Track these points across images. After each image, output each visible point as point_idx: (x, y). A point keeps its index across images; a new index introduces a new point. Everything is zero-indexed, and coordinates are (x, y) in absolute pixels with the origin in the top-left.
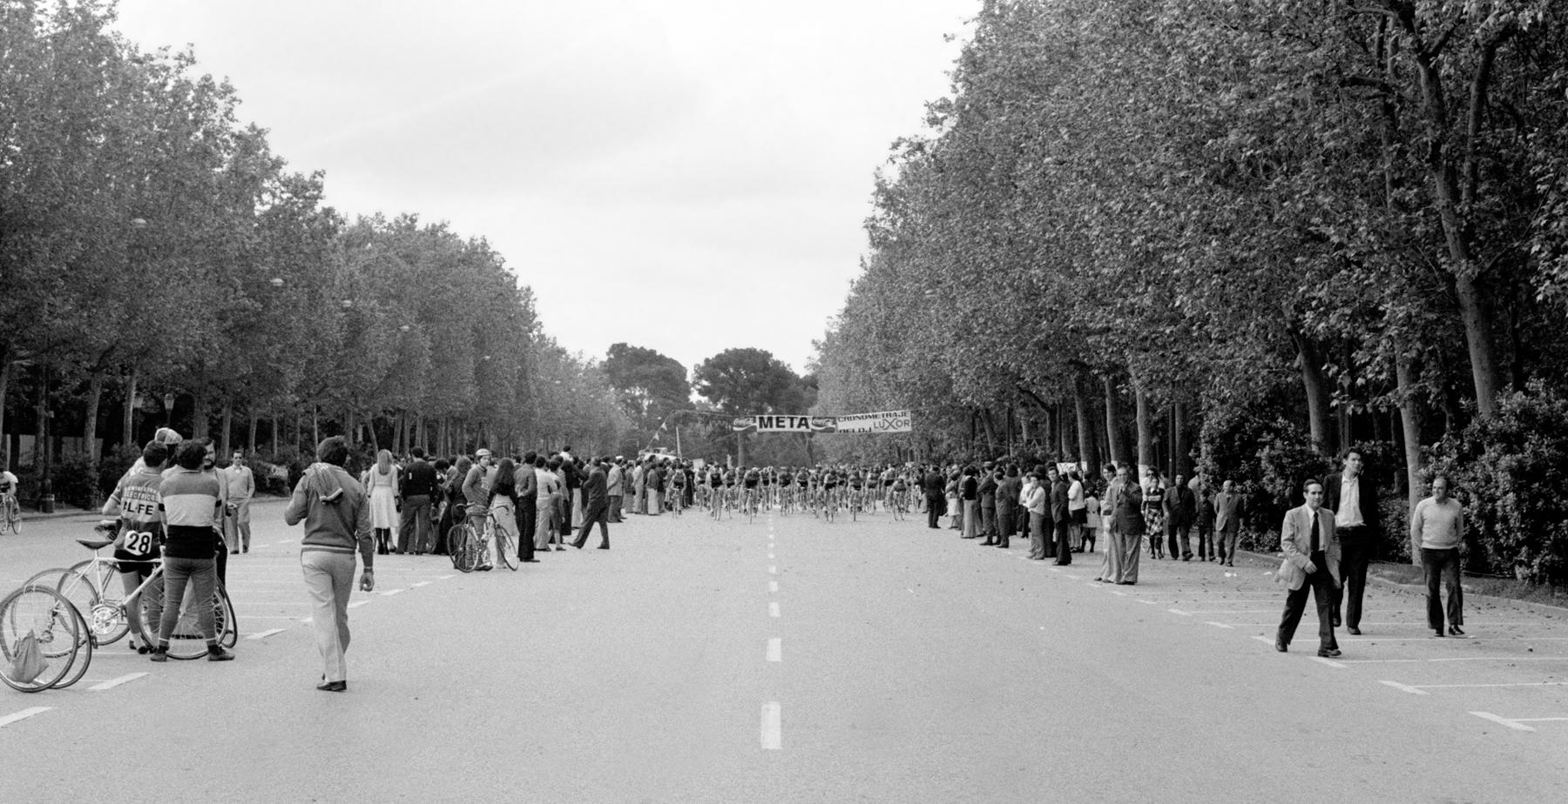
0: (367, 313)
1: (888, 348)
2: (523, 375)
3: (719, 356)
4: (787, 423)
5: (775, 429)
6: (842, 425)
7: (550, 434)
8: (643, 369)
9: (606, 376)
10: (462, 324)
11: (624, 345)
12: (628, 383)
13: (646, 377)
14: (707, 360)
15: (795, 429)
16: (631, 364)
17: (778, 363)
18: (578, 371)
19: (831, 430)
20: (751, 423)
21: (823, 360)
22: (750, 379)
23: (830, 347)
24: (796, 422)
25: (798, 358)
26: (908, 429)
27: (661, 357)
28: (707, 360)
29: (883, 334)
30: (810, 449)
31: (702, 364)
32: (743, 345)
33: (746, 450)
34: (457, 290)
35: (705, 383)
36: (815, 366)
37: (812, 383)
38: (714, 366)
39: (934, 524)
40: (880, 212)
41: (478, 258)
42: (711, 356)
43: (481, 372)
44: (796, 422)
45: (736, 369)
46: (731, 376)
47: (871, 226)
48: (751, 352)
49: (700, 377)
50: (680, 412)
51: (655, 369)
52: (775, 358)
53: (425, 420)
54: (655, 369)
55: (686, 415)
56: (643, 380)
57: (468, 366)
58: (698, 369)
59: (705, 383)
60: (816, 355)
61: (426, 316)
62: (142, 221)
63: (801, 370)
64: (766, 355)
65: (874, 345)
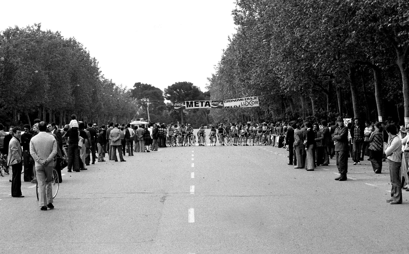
0: (15, 64)
1: (244, 71)
2: (95, 93)
3: (173, 85)
4: (200, 104)
5: (194, 107)
6: (226, 105)
7: (110, 115)
8: (147, 92)
9: (131, 94)
10: (64, 71)
11: (139, 83)
12: (142, 97)
13: (148, 94)
14: (169, 87)
15: (204, 107)
16: (143, 90)
17: (195, 87)
18: (120, 92)
19: (220, 107)
20: (183, 105)
21: (211, 85)
22: (184, 92)
23: (214, 80)
24: (204, 104)
25: (203, 86)
26: (257, 105)
27: (153, 87)
28: (169, 87)
29: (242, 64)
30: (208, 119)
31: (167, 88)
32: (182, 81)
33: (184, 119)
34: (61, 58)
35: (168, 95)
36: (209, 87)
37: (208, 95)
38: (171, 89)
39: (379, 172)
40: (239, 8)
41: (72, 45)
42: (170, 85)
43: (75, 92)
44: (204, 104)
45: (180, 90)
46: (178, 92)
47: (235, 12)
48: (185, 83)
49: (167, 93)
50: (160, 106)
51: (151, 91)
52: (194, 85)
53: (53, 111)
54: (151, 91)
55: (162, 107)
56: (147, 96)
57: (69, 89)
58: (166, 90)
59: (168, 95)
60: (209, 83)
61: (48, 67)
62: (37, 71)
63: (204, 90)
64: (191, 84)
65: (237, 69)
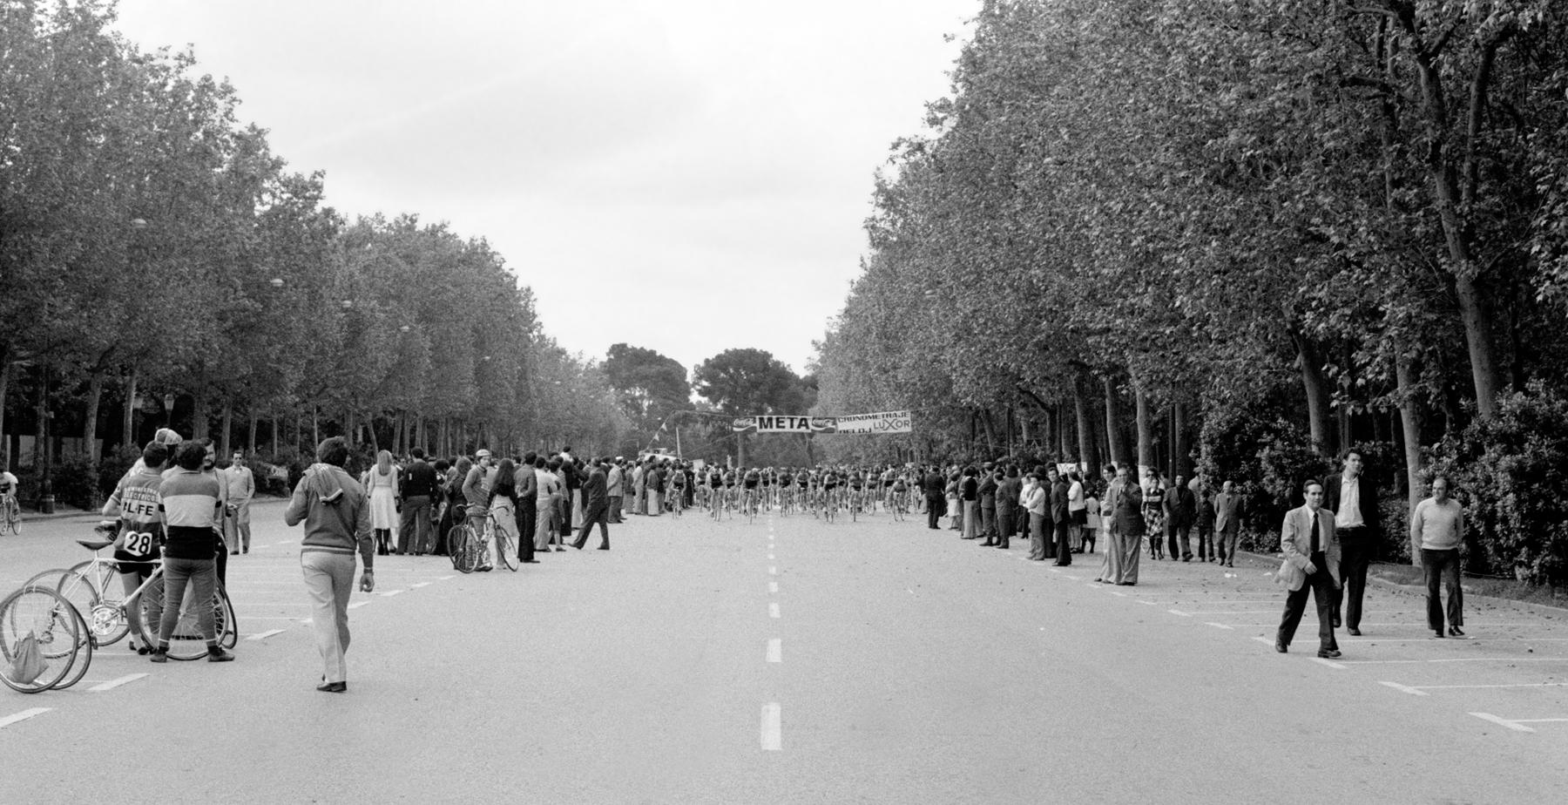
0: (367, 313)
1: (888, 349)
2: (523, 376)
3: (719, 357)
4: (787, 423)
5: (775, 429)
6: (842, 426)
7: (550, 435)
8: (643, 369)
9: (606, 377)
10: (462, 324)
11: (624, 345)
12: (628, 384)
13: (646, 377)
14: (707, 361)
15: (795, 429)
16: (631, 364)
17: (778, 363)
18: (578, 371)
19: (831, 431)
20: (751, 424)
21: (823, 360)
22: (750, 380)
23: (830, 348)
24: (796, 423)
25: (798, 359)
26: (908, 429)
27: (661, 357)
28: (707, 361)
29: (883, 335)
30: (810, 450)
31: (702, 364)
32: (743, 345)
33: (746, 451)
34: (457, 291)
35: (705, 383)
36: (815, 367)
37: (812, 384)
38: (714, 366)
40: (880, 213)
41: (478, 258)
42: (711, 356)
43: (481, 373)
44: (796, 423)
45: (736, 370)
46: (731, 377)
47: (871, 226)
48: (751, 353)
49: (700, 378)
50: (680, 412)
51: (655, 369)
52: (775, 358)
53: (425, 420)
54: (655, 369)
55: (686, 416)
56: (643, 380)
57: (468, 367)
58: (698, 369)
59: (705, 383)
60: (816, 356)
61: (426, 317)
62: (142, 221)
63: (801, 370)
64: (766, 356)
65: (874, 345)
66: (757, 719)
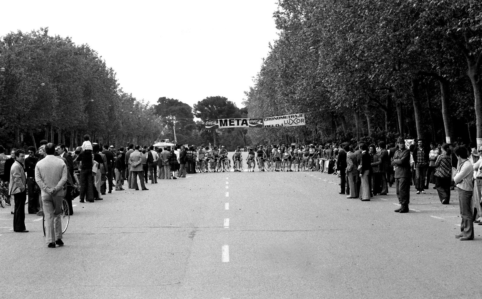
0: (18, 75)
1: (287, 84)
2: (112, 109)
3: (204, 100)
4: (236, 123)
5: (229, 126)
6: (267, 123)
7: (130, 135)
8: (173, 108)
9: (155, 111)
10: (76, 83)
11: (164, 98)
12: (167, 114)
13: (174, 111)
14: (199, 102)
15: (240, 126)
16: (168, 106)
17: (230, 102)
18: (142, 108)
19: (260, 126)
20: (215, 124)
21: (249, 100)
22: (217, 108)
23: (252, 94)
24: (240, 122)
25: (239, 101)
26: (303, 124)
27: (181, 102)
28: (199, 102)
29: (285, 75)
30: (245, 140)
31: (197, 104)
32: (214, 95)
33: (217, 141)
34: (72, 68)
35: (198, 112)
36: (246, 103)
37: (245, 111)
38: (202, 105)
40: (281, 10)
41: (84, 52)
42: (201, 100)
43: (89, 108)
44: (240, 122)
45: (212, 106)
46: (210, 108)
47: (277, 14)
48: (218, 98)
49: (196, 110)
50: (189, 125)
51: (177, 108)
52: (228, 100)
53: (63, 131)
54: (177, 108)
55: (191, 126)
56: (173, 113)
57: (81, 104)
58: (195, 106)
59: (198, 112)
60: (246, 98)
61: (57, 79)
62: (43, 84)
63: (240, 106)
64: (225, 99)
65: (279, 82)
66: (221, 251)
